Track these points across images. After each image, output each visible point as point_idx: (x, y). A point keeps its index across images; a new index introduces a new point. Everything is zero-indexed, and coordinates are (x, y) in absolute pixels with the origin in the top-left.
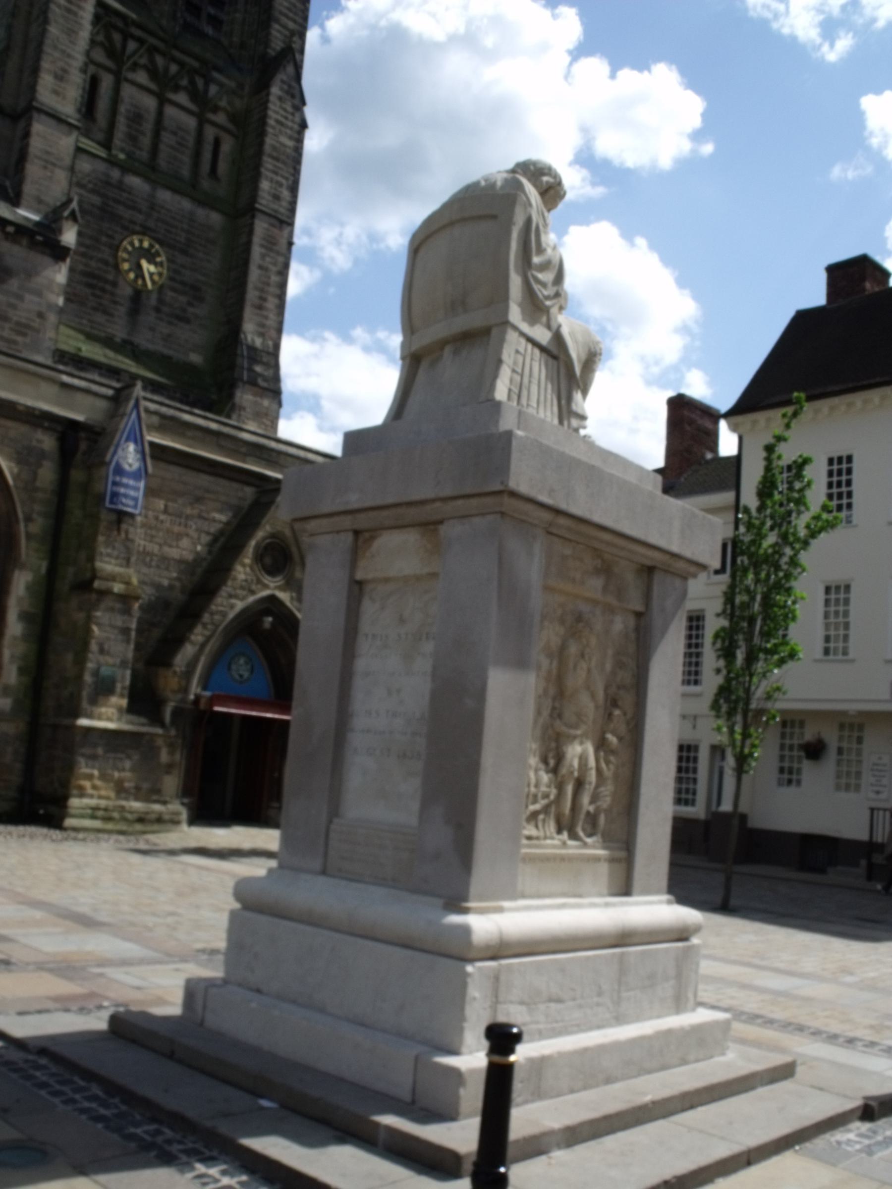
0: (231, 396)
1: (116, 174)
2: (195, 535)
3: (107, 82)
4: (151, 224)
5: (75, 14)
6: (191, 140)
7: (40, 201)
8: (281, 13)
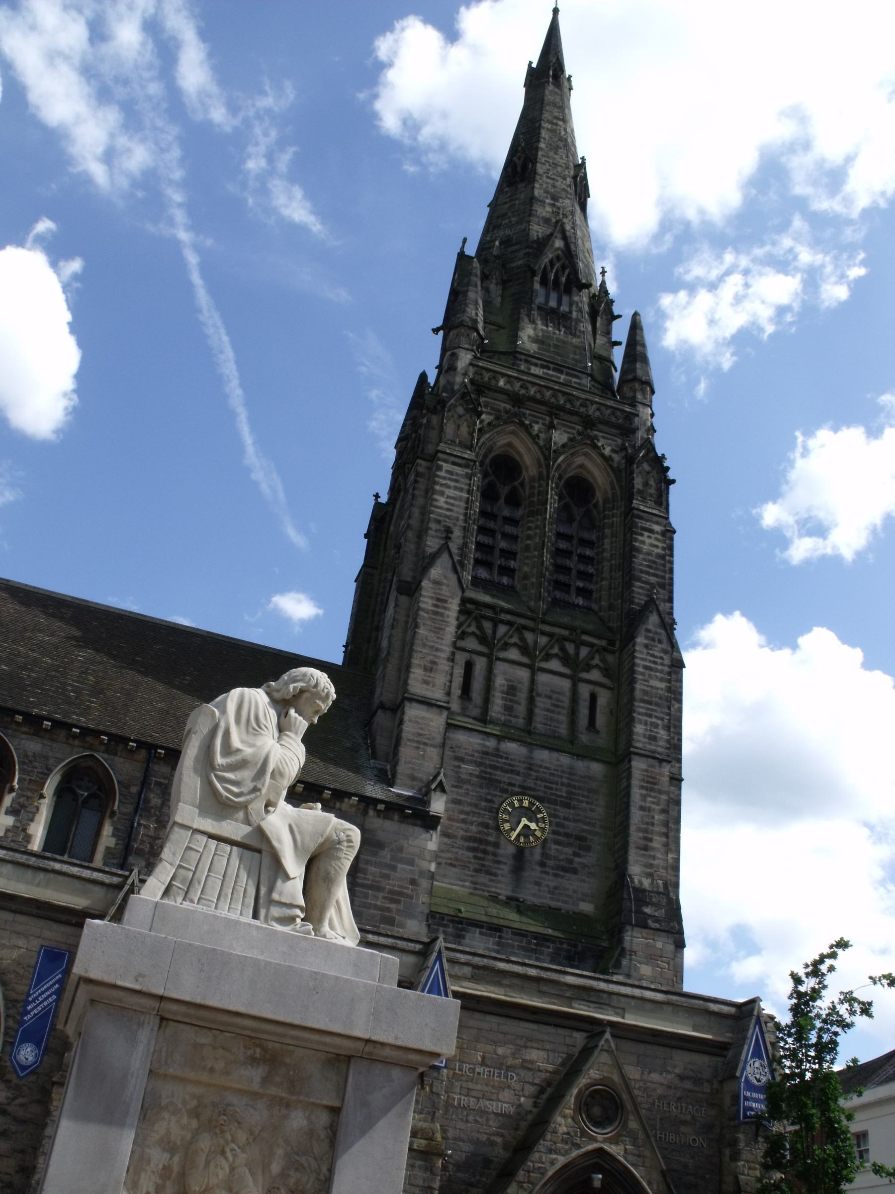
0: (620, 941)
1: (491, 743)
2: (518, 1087)
3: (480, 664)
4: (530, 783)
5: (442, 615)
6: (566, 701)
7: (414, 778)
8: (642, 571)
